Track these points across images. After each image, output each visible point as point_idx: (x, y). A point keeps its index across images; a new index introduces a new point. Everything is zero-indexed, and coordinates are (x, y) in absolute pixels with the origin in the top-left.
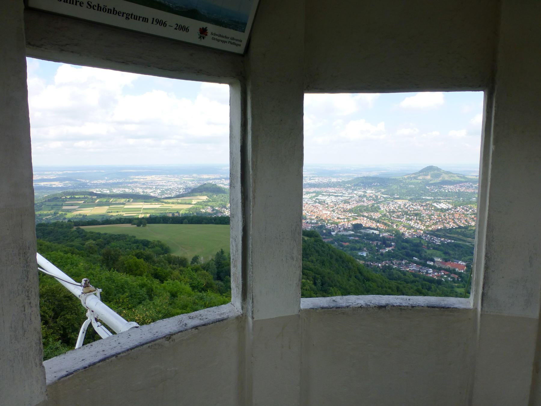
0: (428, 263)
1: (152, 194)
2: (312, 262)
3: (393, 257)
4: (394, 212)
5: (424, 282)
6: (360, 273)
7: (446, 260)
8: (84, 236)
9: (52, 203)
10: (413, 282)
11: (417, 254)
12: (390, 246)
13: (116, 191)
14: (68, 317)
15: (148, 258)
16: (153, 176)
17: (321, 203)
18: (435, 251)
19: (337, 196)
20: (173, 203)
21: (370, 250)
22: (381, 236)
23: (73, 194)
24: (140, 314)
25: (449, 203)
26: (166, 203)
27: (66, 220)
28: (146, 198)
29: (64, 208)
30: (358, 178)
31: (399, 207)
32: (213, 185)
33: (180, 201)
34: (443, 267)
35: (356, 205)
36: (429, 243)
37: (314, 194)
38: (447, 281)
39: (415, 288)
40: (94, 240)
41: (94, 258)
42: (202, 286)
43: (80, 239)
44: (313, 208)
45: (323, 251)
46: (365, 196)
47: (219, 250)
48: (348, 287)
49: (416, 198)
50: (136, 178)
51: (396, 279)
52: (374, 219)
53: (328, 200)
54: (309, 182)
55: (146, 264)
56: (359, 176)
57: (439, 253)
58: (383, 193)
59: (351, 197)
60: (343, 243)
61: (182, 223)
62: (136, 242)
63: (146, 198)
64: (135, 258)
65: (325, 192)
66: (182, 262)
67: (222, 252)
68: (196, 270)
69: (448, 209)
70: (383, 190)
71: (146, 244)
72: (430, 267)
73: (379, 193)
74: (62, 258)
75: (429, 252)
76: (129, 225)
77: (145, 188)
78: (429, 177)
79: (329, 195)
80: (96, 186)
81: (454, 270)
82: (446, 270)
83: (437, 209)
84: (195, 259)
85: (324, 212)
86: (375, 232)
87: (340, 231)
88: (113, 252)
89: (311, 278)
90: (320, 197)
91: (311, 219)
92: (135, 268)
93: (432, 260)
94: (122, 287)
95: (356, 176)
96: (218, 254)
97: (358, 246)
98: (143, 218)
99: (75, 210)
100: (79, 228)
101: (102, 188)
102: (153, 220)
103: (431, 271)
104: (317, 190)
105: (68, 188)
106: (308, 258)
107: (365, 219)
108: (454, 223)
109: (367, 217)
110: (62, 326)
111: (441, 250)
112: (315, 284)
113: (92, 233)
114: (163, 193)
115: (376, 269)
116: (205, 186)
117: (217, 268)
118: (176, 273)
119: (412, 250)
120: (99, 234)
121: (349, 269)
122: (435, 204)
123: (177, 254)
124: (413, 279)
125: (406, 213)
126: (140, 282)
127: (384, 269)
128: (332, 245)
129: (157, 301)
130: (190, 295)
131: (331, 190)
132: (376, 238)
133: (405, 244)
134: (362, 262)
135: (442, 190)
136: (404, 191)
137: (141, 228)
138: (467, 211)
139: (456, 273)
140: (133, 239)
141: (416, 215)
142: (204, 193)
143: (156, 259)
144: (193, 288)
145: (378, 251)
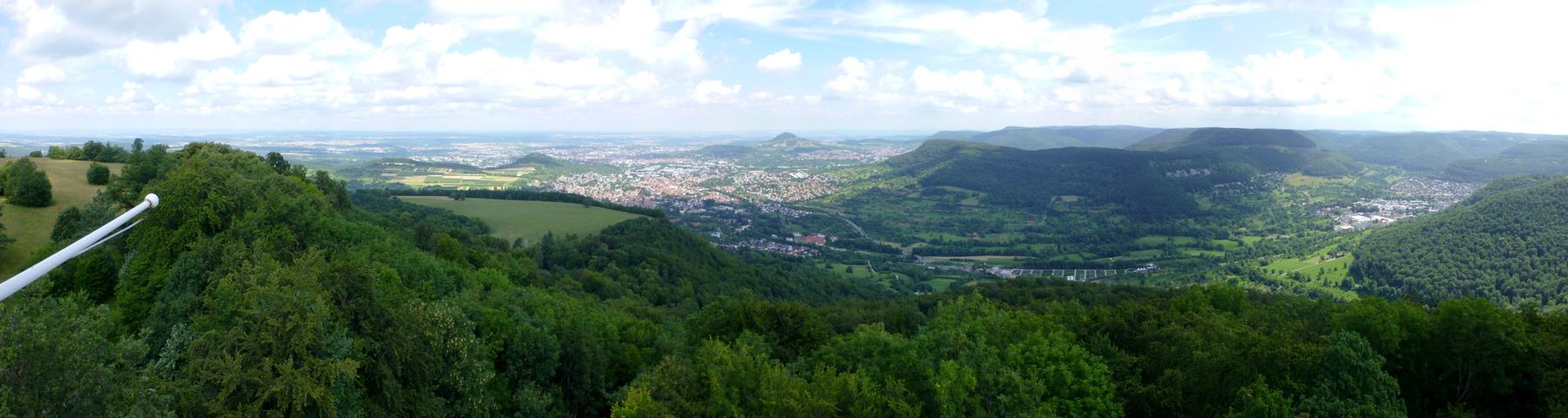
0: (788, 239)
1: (472, 164)
2: (658, 247)
3: (750, 236)
4: (749, 184)
5: (784, 262)
6: (714, 258)
7: (805, 235)
8: (400, 207)
9: (372, 170)
10: (773, 262)
11: (776, 231)
12: (747, 223)
13: (435, 159)
14: (361, 301)
15: (463, 238)
16: (475, 144)
17: (668, 176)
18: (793, 226)
19: (686, 168)
20: (495, 175)
21: (725, 230)
22: (736, 212)
23: (393, 160)
24: (440, 310)
25: (805, 172)
26: (488, 174)
27: (384, 188)
28: (468, 169)
29: (383, 175)
30: (708, 147)
31: (755, 179)
32: (542, 155)
33: (503, 173)
34: (803, 242)
35: (707, 178)
36: (787, 216)
37: (659, 166)
38: (807, 258)
39: (775, 269)
40: (410, 212)
41: (407, 232)
42: (524, 277)
43: (396, 210)
44: (657, 182)
45: (670, 234)
46: (717, 167)
47: (546, 233)
48: (700, 276)
49: (772, 170)
50: (456, 146)
51: (754, 262)
52: (728, 194)
53: (675, 172)
54: (652, 151)
55: (460, 245)
56: (710, 145)
57: (798, 227)
58: (736, 164)
59: (702, 169)
60: (694, 224)
61: (504, 199)
62: (453, 217)
63: (468, 169)
64: (449, 236)
65: (672, 163)
66: (502, 246)
67: (550, 235)
68: (518, 256)
69: (805, 179)
70: (736, 160)
71: (463, 220)
72: (790, 243)
73: (732, 164)
74: (370, 230)
75: (788, 227)
76: (446, 198)
77: (466, 157)
78: (784, 145)
79: (677, 167)
80: (416, 154)
81: (814, 244)
82: (805, 245)
83: (793, 179)
84: (518, 242)
85: (671, 187)
86: (729, 208)
87: (689, 209)
88: (426, 228)
89: (656, 267)
90: (666, 170)
91: (657, 196)
92: (448, 249)
93: (792, 236)
94: (427, 271)
95: (706, 144)
96: (545, 237)
97: (710, 225)
98: (462, 191)
99: (393, 177)
100: (395, 198)
101: (422, 156)
102: (472, 194)
103: (790, 248)
104: (663, 161)
105: (388, 154)
106: (652, 243)
107: (718, 193)
108: (812, 193)
109: (720, 192)
110: (354, 311)
111: (801, 224)
112: (661, 274)
113: (407, 203)
114: (485, 163)
115: (731, 252)
116: (533, 156)
117: (544, 254)
118: (494, 258)
119: (770, 227)
120: (415, 205)
121: (702, 254)
122: (792, 174)
123: (497, 235)
124: (773, 259)
125: (762, 185)
126: (449, 268)
127: (742, 251)
128: (681, 226)
129: (466, 294)
130: (505, 289)
131: (679, 161)
132: (730, 215)
133: (762, 220)
134: (715, 245)
135: (798, 158)
136: (759, 161)
137: (459, 202)
138: (823, 179)
139: (815, 248)
140: (450, 214)
141: (773, 186)
142: (533, 164)
143: (472, 239)
144: (513, 277)
145: (733, 230)
